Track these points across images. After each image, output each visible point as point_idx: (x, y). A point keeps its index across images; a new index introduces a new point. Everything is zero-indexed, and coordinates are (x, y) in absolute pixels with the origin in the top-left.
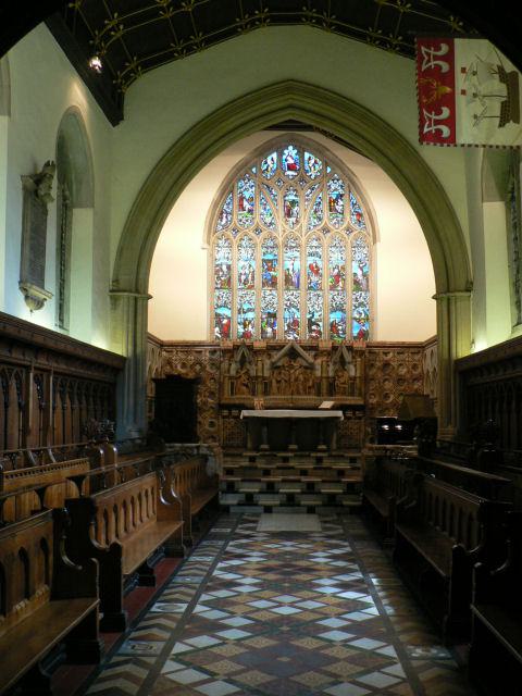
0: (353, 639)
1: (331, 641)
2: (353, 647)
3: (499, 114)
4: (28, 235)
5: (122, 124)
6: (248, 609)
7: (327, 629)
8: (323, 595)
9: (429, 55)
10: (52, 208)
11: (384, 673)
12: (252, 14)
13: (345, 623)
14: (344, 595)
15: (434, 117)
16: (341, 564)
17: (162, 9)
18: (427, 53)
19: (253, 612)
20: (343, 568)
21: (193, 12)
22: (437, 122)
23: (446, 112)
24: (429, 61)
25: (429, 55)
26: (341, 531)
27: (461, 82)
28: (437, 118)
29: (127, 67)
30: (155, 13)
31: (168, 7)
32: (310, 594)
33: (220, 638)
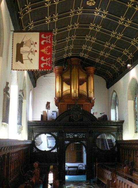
3: (24, 61)
8: (84, 186)
9: (48, 40)
10: (49, 127)
11: (47, 141)
12: (118, 33)
15: (47, 64)
18: (49, 41)
22: (45, 62)
23: (42, 43)
24: (48, 38)
25: (48, 63)
27: (37, 47)
28: (45, 63)
29: (47, 65)
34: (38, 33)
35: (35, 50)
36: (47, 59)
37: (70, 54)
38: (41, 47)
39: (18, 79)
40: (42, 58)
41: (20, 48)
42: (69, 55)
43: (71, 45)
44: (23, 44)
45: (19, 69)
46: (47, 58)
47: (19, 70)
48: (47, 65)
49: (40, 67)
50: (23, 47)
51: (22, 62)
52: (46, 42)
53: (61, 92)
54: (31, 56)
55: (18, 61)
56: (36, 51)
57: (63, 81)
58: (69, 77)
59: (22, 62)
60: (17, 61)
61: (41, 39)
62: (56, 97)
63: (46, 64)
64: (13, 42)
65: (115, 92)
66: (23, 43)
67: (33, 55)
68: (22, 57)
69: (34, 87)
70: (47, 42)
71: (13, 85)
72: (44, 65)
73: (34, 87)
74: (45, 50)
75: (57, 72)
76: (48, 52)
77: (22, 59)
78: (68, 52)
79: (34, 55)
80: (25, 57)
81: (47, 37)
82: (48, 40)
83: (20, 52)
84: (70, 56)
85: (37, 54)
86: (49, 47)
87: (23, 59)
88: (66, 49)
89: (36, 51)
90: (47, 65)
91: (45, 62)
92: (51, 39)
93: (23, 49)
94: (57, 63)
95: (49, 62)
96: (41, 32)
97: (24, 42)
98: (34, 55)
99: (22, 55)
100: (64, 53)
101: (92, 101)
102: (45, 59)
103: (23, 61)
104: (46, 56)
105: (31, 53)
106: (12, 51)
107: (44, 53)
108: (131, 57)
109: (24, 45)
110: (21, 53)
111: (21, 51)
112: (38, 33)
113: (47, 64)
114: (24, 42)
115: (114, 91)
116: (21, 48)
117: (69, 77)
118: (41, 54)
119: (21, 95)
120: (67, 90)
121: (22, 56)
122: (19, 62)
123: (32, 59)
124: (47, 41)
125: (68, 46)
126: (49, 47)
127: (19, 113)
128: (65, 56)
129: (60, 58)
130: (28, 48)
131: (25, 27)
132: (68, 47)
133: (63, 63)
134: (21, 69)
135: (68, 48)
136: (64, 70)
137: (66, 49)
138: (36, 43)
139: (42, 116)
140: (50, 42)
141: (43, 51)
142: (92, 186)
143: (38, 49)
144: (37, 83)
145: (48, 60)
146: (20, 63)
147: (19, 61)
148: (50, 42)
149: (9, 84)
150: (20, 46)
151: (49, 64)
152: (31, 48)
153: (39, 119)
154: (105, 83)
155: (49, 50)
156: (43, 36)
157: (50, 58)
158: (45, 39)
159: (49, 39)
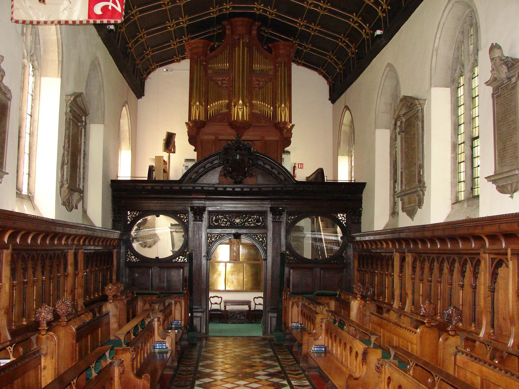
0: (269, 378)
1: (261, 379)
2: (269, 381)
4: (452, 108)
5: (399, 384)
6: (223, 368)
7: (258, 375)
8: (261, 380)
13: (261, 357)
14: (271, 380)
16: (268, 362)
17: (164, 4)
19: (225, 369)
20: (270, 365)
21: (184, 5)
26: (279, 368)
29: (112, 7)
30: (160, 6)
31: (168, 3)
32: (254, 380)
33: (213, 379)
49: (91, 13)
63: (108, 6)
65: (349, 110)
71: (46, 76)
90: (112, 7)
101: (285, 131)
108: (385, 9)
115: (347, 108)
127: (66, 153)
139: (151, 170)
142: (285, 382)
149: (365, 187)
151: (117, 5)
153: (144, 175)
154: (327, 88)
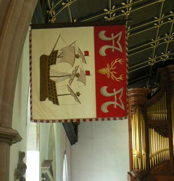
3: (59, 98)
9: (117, 46)
15: (115, 103)
18: (117, 46)
22: (111, 99)
23: (103, 51)
24: (116, 40)
25: (118, 101)
27: (90, 64)
34: (91, 29)
35: (86, 71)
36: (115, 93)
37: (166, 56)
38: (100, 62)
39: (38, 135)
40: (104, 90)
41: (49, 65)
42: (163, 58)
43: (168, 35)
44: (56, 56)
45: (48, 118)
46: (115, 90)
47: (42, 121)
48: (115, 107)
50: (55, 63)
51: (56, 102)
52: (111, 49)
53: (144, 157)
54: (76, 86)
55: (45, 100)
56: (88, 73)
57: (149, 126)
58: (165, 116)
59: (56, 102)
60: (42, 99)
61: (98, 43)
62: (132, 169)
64: (30, 52)
66: (54, 54)
67: (81, 83)
68: (55, 90)
69: (72, 143)
70: (113, 51)
72: (110, 108)
73: (72, 143)
74: (111, 71)
75: (133, 104)
76: (117, 76)
77: (56, 93)
78: (159, 51)
79: (85, 83)
80: (61, 87)
81: (113, 38)
82: (117, 46)
83: (49, 77)
84: (165, 60)
85: (91, 80)
86: (119, 61)
87: (58, 93)
88: (155, 43)
89: (88, 73)
91: (111, 99)
92: (122, 42)
93: (58, 69)
94: (135, 79)
95: (120, 98)
96: (99, 25)
97: (57, 52)
98: (85, 83)
99: (54, 83)
100: (149, 54)
102: (110, 90)
103: (57, 99)
104: (112, 85)
105: (76, 78)
106: (31, 75)
107: (108, 77)
109: (58, 60)
110: (51, 78)
111: (51, 75)
112: (91, 29)
113: (115, 103)
114: (57, 52)
116: (52, 67)
117: (165, 116)
118: (101, 81)
119: (46, 173)
120: (164, 150)
121: (55, 87)
122: (48, 102)
123: (78, 94)
124: (113, 47)
125: (161, 37)
126: (119, 61)
128: (152, 61)
129: (140, 66)
130: (69, 65)
131: (54, 5)
132: (158, 39)
133: (148, 77)
134: (53, 118)
135: (161, 42)
136: (149, 97)
137: (155, 43)
138: (87, 53)
140: (121, 50)
141: (104, 71)
143: (92, 69)
144: (79, 133)
145: (118, 95)
146: (51, 102)
147: (47, 99)
148: (121, 50)
150: (47, 61)
151: (120, 103)
152: (76, 64)
155: (119, 70)
156: (102, 35)
157: (121, 90)
158: (110, 43)
159: (118, 42)
